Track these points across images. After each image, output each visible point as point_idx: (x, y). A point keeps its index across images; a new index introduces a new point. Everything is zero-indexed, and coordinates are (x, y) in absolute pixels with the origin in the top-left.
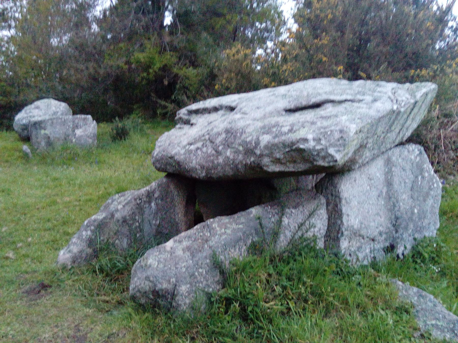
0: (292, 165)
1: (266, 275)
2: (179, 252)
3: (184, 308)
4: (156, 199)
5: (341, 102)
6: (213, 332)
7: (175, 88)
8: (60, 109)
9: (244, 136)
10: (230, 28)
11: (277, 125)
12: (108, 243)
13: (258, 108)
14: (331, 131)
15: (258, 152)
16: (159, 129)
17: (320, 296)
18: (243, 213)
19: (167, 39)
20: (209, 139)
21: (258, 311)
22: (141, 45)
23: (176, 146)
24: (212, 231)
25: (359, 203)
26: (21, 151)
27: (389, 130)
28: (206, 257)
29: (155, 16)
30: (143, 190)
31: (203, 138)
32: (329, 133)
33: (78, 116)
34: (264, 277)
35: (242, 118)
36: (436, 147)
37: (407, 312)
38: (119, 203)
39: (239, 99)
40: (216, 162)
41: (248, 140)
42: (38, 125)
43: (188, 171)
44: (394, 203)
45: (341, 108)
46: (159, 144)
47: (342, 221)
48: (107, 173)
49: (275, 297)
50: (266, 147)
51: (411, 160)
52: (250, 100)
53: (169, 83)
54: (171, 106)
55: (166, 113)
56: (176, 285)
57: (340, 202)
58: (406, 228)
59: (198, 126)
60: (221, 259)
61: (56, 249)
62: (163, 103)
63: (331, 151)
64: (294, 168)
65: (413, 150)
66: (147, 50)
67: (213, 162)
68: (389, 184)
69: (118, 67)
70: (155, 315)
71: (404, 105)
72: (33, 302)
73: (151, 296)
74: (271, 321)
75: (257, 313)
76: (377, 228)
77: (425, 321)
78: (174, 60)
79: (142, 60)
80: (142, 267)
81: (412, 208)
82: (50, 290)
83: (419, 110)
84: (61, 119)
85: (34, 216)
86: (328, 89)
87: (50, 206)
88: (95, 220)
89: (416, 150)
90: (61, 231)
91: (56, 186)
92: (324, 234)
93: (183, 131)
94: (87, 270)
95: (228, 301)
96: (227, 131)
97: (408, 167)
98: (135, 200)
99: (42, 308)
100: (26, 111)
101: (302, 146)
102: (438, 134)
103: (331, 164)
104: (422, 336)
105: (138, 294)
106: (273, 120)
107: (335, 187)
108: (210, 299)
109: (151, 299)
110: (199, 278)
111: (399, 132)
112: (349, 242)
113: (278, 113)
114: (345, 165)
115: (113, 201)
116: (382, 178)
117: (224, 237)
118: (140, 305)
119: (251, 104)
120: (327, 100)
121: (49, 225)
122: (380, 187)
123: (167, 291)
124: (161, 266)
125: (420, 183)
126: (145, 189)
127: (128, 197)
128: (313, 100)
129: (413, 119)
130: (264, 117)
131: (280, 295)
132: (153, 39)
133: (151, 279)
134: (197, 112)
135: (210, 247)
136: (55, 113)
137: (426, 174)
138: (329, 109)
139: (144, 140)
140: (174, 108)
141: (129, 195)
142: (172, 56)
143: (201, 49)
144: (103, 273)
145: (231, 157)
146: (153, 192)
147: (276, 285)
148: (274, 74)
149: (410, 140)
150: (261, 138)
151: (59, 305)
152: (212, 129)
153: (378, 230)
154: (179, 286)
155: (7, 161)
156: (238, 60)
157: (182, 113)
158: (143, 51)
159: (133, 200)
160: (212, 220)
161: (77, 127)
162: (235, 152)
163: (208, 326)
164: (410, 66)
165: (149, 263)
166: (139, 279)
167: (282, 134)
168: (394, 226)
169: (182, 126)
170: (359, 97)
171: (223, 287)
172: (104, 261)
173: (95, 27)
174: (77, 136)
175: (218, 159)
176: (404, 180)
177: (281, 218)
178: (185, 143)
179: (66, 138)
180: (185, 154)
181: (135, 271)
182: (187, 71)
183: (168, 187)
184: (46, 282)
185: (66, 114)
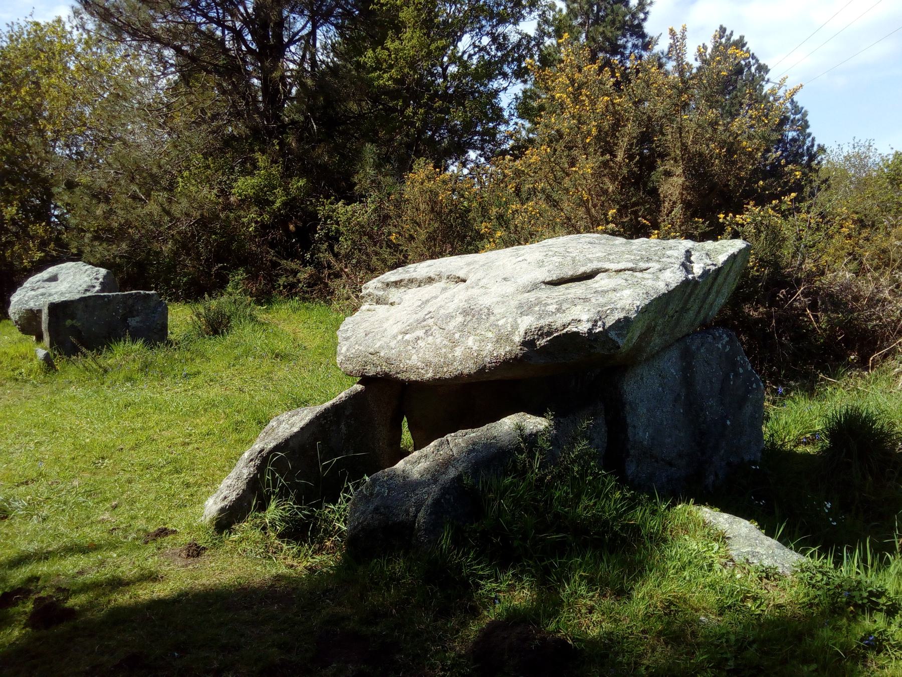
25: (648, 411)
39: (468, 264)
52: (487, 266)
65: (721, 336)
83: (725, 279)
106: (532, 296)
112: (638, 466)
128: (581, 270)
129: (718, 292)
134: (397, 284)
137: (741, 371)
138: (600, 282)
157: (372, 286)
170: (643, 265)
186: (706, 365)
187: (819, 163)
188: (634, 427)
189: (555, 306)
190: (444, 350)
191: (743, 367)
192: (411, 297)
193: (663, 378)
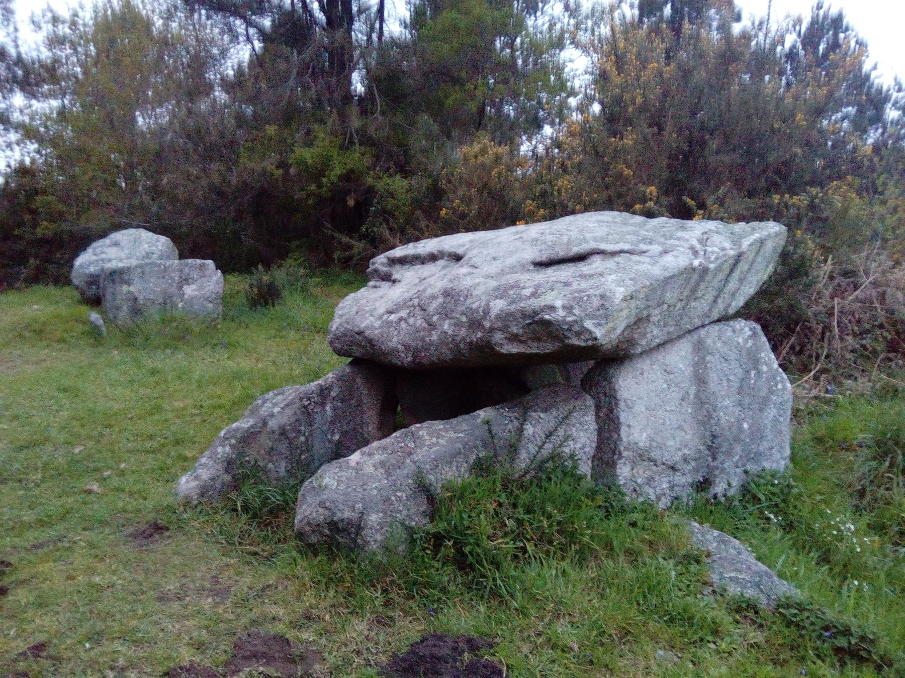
0: (535, 344)
1: (495, 504)
2: (369, 469)
3: (374, 546)
4: (334, 399)
5: (614, 254)
6: (415, 583)
7: (368, 211)
8: (157, 246)
9: (469, 301)
10: (473, 107)
11: (516, 286)
12: (256, 466)
13: (495, 259)
14: (588, 296)
15: (487, 324)
16: (337, 287)
17: (572, 536)
18: (467, 417)
19: (355, 122)
20: (419, 305)
21: (480, 551)
22: (308, 133)
23: (367, 315)
24: (418, 440)
26: (85, 322)
27: (693, 295)
28: (408, 476)
29: (334, 80)
30: (313, 385)
31: (410, 303)
32: (585, 298)
33: (190, 261)
34: (491, 507)
35: (470, 274)
36: (827, 328)
37: (698, 561)
38: (275, 405)
39: (471, 241)
40: (427, 339)
41: (474, 306)
42: (117, 276)
43: (384, 354)
44: (708, 412)
45: (611, 263)
46: (340, 312)
47: (619, 435)
48: (244, 363)
49: (506, 534)
50: (498, 317)
51: (738, 343)
52: (484, 244)
53: (357, 203)
54: (359, 246)
55: (351, 258)
56: (363, 513)
57: (617, 404)
58: (729, 453)
59: (403, 283)
60: (430, 480)
61: (167, 481)
62: (345, 239)
63: (589, 324)
64: (538, 348)
66: (318, 142)
67: (423, 340)
68: (700, 380)
69: (264, 172)
70: (332, 558)
71: (717, 259)
72: (144, 548)
73: (327, 531)
74: (497, 566)
75: (478, 555)
76: (679, 449)
77: (721, 573)
78: (367, 160)
79: (310, 161)
80: (314, 488)
81: (739, 421)
82: (167, 533)
84: (160, 264)
85: (125, 429)
86: (600, 232)
87: (151, 414)
88: (237, 430)
89: (747, 329)
90: (173, 454)
91: (157, 383)
92: (592, 454)
93: (380, 292)
94: (223, 508)
95: (438, 539)
96: (446, 293)
97: (733, 356)
98: (301, 399)
99: (159, 556)
100: (95, 248)
101: (547, 317)
102: (830, 306)
103: (590, 343)
104: (714, 592)
105: (307, 529)
106: (511, 278)
107: (610, 383)
108: (411, 536)
109: (327, 536)
110: (396, 504)
111: (715, 301)
112: (632, 469)
113: (523, 268)
114: (618, 346)
115: (264, 402)
116: (688, 372)
117: (434, 449)
118: (310, 546)
119: (485, 253)
120: (596, 249)
121: (149, 444)
122: (686, 385)
123: (350, 522)
124: (342, 486)
125: (752, 382)
126: (316, 383)
127: (289, 395)
128: (575, 250)
129: (741, 280)
130: (502, 273)
131: (513, 532)
132: (330, 122)
133: (328, 504)
134: (403, 261)
135: (414, 462)
136: (149, 255)
137: (765, 368)
138: (596, 264)
139: (308, 307)
140: (365, 250)
141: (291, 392)
142: (363, 154)
143: (418, 142)
144: (248, 513)
145: (450, 332)
146: (329, 388)
147: (508, 519)
148: (544, 194)
149: (738, 315)
150: (492, 304)
151: (184, 552)
152: (424, 290)
153: (680, 454)
154: (368, 515)
155: (62, 341)
156: (483, 165)
157: (380, 261)
158: (311, 145)
159: (297, 401)
160: (418, 425)
161: (186, 280)
162: (456, 325)
163: (408, 574)
164: (772, 187)
165: (324, 484)
166: (310, 506)
167: (521, 299)
168: (709, 448)
169: (378, 284)
170: (643, 247)
171: (432, 521)
172: (250, 493)
173: (220, 96)
174: (186, 297)
175: (431, 335)
176: (726, 375)
177: (522, 424)
178: (381, 310)
179: (167, 302)
180: (381, 327)
181: (303, 495)
182: (389, 181)
183: (354, 380)
184: (162, 523)
185: (168, 258)
186: (722, 360)
187: (357, 41)
188: (629, 426)
189: (531, 290)
190: (422, 333)
191: (767, 365)
192: (408, 276)
193: (669, 373)
